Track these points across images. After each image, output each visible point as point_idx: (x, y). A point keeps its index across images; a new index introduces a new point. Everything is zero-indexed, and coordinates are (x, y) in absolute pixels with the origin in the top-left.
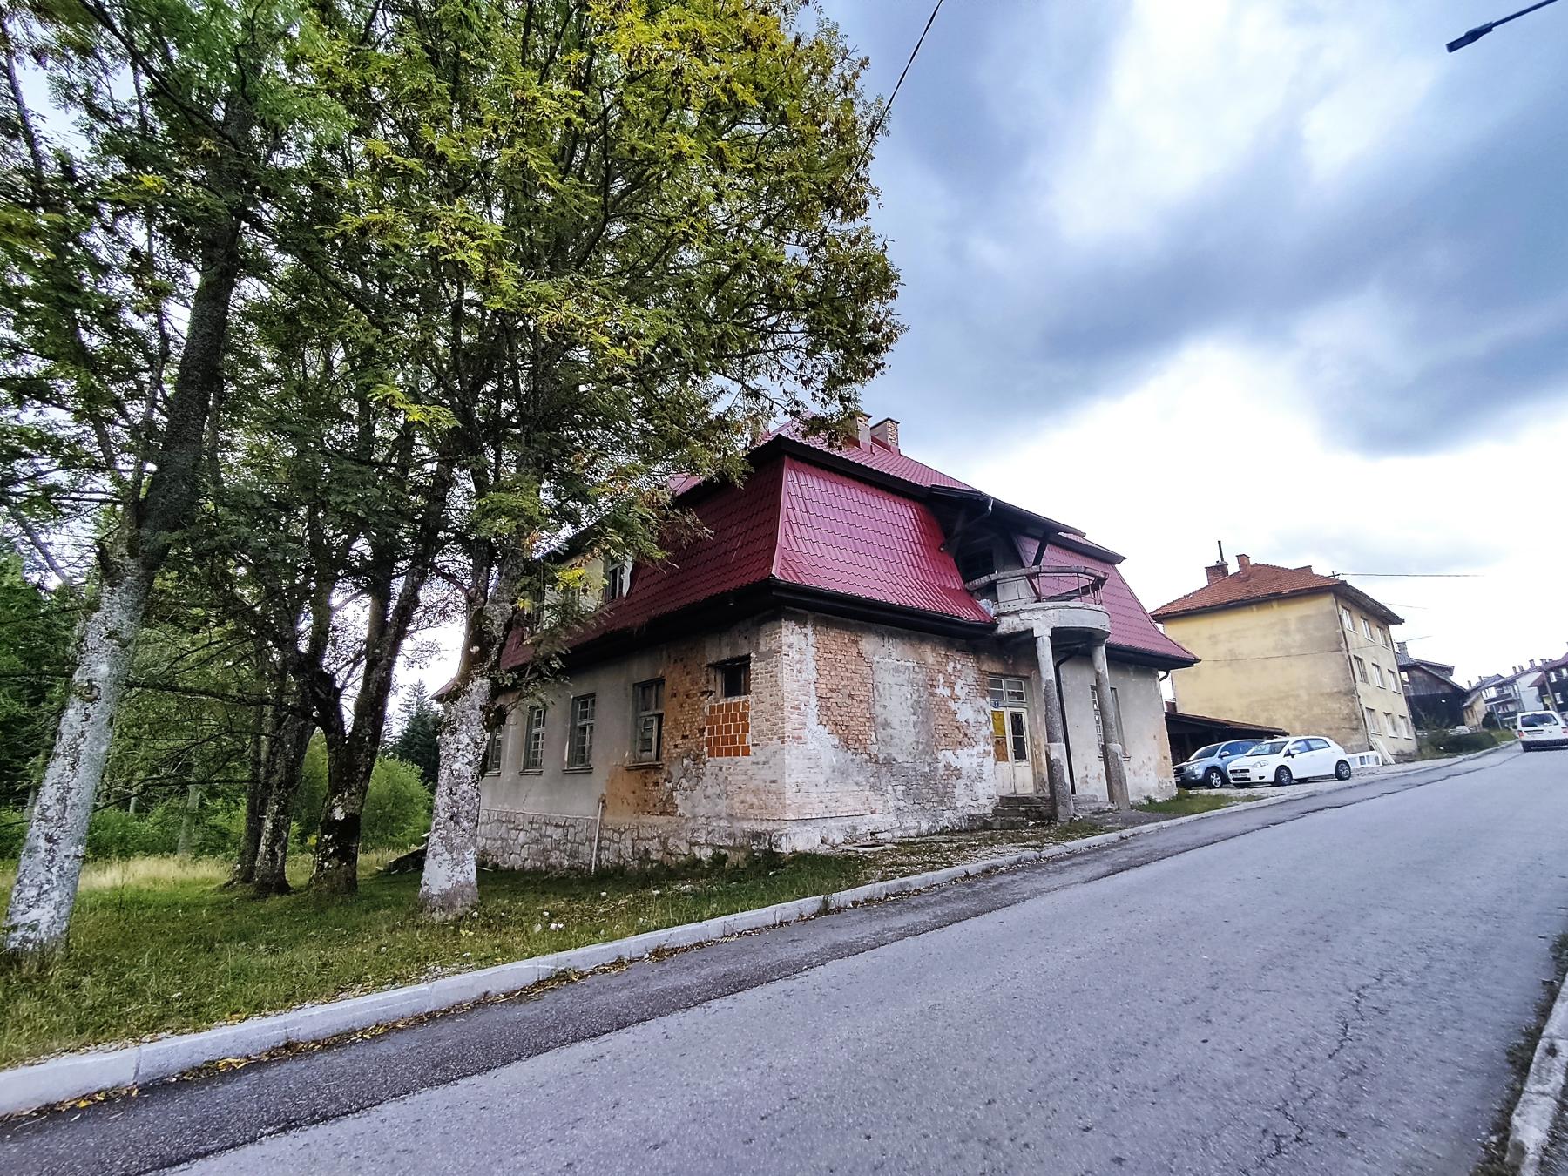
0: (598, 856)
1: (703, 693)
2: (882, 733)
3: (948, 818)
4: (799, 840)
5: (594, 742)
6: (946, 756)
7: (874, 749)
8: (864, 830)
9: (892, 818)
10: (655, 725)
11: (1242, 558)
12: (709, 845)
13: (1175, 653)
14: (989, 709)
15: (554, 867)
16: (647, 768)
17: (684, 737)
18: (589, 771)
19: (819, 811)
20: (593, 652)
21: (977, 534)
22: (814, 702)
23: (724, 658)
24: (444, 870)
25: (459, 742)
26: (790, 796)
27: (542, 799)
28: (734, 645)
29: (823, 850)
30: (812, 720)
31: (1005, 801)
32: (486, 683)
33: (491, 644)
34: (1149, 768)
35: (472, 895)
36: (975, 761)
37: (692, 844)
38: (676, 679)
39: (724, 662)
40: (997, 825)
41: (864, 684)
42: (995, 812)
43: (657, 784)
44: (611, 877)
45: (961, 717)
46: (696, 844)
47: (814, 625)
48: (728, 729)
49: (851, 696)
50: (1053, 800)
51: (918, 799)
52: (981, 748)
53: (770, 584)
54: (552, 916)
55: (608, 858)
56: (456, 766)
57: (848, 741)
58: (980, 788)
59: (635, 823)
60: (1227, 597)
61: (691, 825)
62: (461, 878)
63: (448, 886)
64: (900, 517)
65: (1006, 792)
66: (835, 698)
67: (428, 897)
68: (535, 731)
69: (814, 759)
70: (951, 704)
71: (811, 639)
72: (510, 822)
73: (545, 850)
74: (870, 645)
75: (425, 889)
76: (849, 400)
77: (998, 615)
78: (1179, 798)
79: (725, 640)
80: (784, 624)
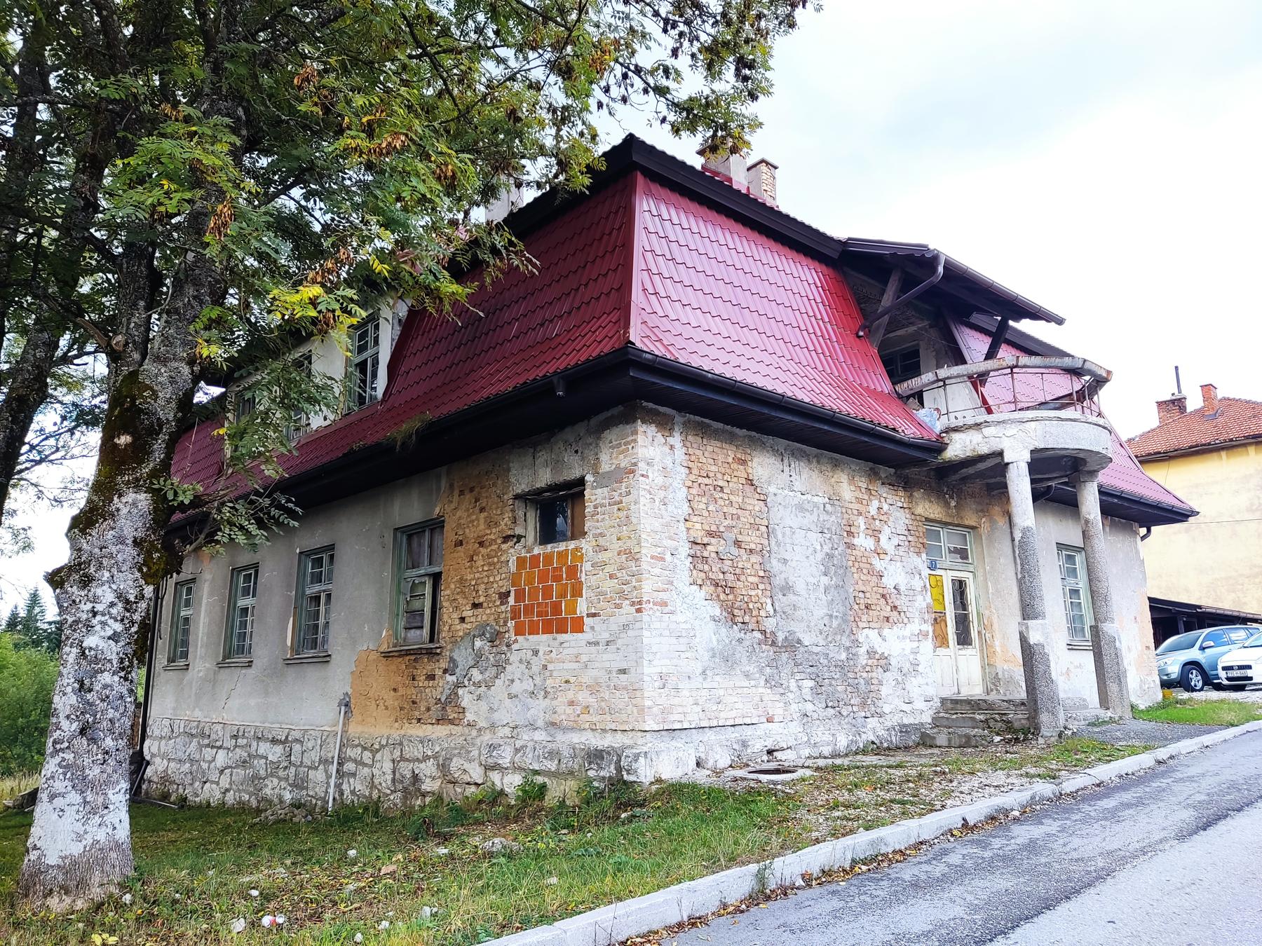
0: (338, 786)
1: (506, 539)
2: (782, 601)
3: (874, 730)
4: (661, 764)
5: (333, 615)
6: (869, 637)
7: (770, 624)
9: (795, 727)
10: (428, 590)
11: (1207, 389)
12: (517, 769)
13: (1167, 500)
14: (926, 572)
15: (270, 802)
16: (418, 651)
17: (476, 606)
18: (326, 659)
19: (694, 718)
20: (332, 482)
21: (916, 306)
22: (685, 549)
23: (541, 484)
24: (70, 822)
25: (96, 600)
26: (651, 695)
27: (252, 702)
28: (557, 464)
29: (702, 777)
31: (952, 705)
32: (143, 500)
33: (154, 432)
34: (1143, 663)
35: (120, 865)
36: (909, 646)
37: (488, 768)
38: (460, 517)
39: (540, 491)
40: (942, 740)
41: (755, 526)
42: (936, 722)
43: (431, 677)
44: (359, 818)
45: (888, 582)
46: (495, 767)
47: (684, 433)
48: (547, 592)
49: (737, 543)
50: (1032, 704)
51: (833, 704)
52: (915, 627)
53: (626, 358)
54: (266, 897)
55: (355, 788)
56: (90, 641)
57: (735, 612)
58: (916, 687)
59: (396, 735)
60: (1186, 441)
61: (487, 738)
62: (101, 836)
63: (76, 849)
64: (801, 281)
65: (948, 692)
66: (715, 545)
67: (39, 870)
68: (242, 603)
70: (876, 561)
71: (680, 452)
72: (203, 735)
73: (256, 777)
75: (33, 855)
76: (751, 66)
77: (949, 430)
78: (1164, 705)
79: (543, 456)
80: (641, 427)
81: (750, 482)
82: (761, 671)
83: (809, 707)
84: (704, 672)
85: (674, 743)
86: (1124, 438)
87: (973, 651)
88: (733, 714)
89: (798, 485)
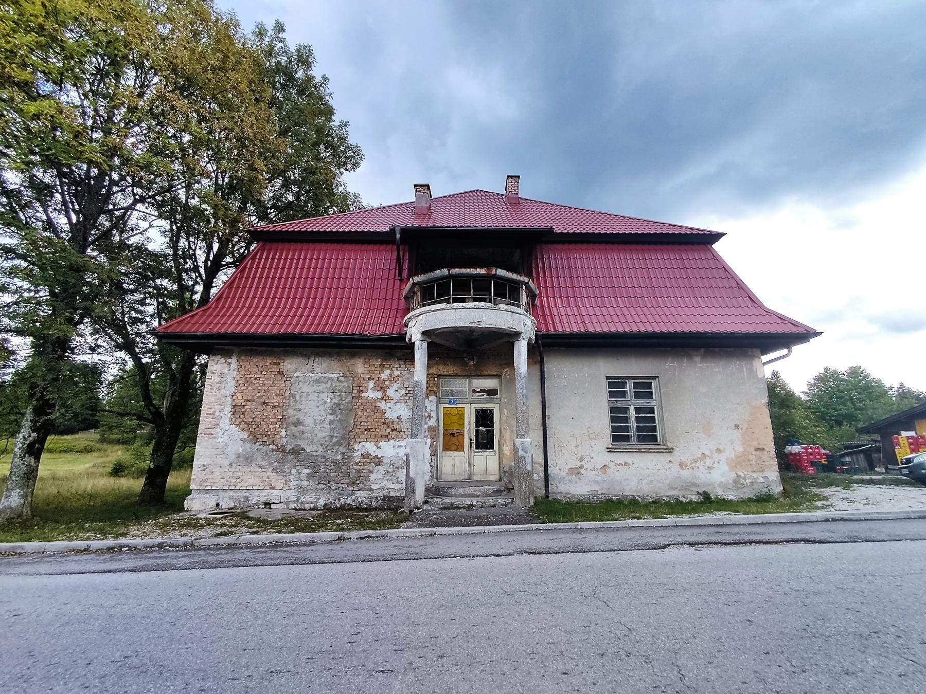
8: (254, 501)
13: (788, 329)
19: (219, 484)
22: (228, 409)
30: (225, 423)
57: (257, 434)
69: (222, 450)
74: (290, 365)
82: (270, 464)
83: (305, 483)
84: (231, 464)
86: (770, 477)
87: (492, 454)
89: (318, 370)
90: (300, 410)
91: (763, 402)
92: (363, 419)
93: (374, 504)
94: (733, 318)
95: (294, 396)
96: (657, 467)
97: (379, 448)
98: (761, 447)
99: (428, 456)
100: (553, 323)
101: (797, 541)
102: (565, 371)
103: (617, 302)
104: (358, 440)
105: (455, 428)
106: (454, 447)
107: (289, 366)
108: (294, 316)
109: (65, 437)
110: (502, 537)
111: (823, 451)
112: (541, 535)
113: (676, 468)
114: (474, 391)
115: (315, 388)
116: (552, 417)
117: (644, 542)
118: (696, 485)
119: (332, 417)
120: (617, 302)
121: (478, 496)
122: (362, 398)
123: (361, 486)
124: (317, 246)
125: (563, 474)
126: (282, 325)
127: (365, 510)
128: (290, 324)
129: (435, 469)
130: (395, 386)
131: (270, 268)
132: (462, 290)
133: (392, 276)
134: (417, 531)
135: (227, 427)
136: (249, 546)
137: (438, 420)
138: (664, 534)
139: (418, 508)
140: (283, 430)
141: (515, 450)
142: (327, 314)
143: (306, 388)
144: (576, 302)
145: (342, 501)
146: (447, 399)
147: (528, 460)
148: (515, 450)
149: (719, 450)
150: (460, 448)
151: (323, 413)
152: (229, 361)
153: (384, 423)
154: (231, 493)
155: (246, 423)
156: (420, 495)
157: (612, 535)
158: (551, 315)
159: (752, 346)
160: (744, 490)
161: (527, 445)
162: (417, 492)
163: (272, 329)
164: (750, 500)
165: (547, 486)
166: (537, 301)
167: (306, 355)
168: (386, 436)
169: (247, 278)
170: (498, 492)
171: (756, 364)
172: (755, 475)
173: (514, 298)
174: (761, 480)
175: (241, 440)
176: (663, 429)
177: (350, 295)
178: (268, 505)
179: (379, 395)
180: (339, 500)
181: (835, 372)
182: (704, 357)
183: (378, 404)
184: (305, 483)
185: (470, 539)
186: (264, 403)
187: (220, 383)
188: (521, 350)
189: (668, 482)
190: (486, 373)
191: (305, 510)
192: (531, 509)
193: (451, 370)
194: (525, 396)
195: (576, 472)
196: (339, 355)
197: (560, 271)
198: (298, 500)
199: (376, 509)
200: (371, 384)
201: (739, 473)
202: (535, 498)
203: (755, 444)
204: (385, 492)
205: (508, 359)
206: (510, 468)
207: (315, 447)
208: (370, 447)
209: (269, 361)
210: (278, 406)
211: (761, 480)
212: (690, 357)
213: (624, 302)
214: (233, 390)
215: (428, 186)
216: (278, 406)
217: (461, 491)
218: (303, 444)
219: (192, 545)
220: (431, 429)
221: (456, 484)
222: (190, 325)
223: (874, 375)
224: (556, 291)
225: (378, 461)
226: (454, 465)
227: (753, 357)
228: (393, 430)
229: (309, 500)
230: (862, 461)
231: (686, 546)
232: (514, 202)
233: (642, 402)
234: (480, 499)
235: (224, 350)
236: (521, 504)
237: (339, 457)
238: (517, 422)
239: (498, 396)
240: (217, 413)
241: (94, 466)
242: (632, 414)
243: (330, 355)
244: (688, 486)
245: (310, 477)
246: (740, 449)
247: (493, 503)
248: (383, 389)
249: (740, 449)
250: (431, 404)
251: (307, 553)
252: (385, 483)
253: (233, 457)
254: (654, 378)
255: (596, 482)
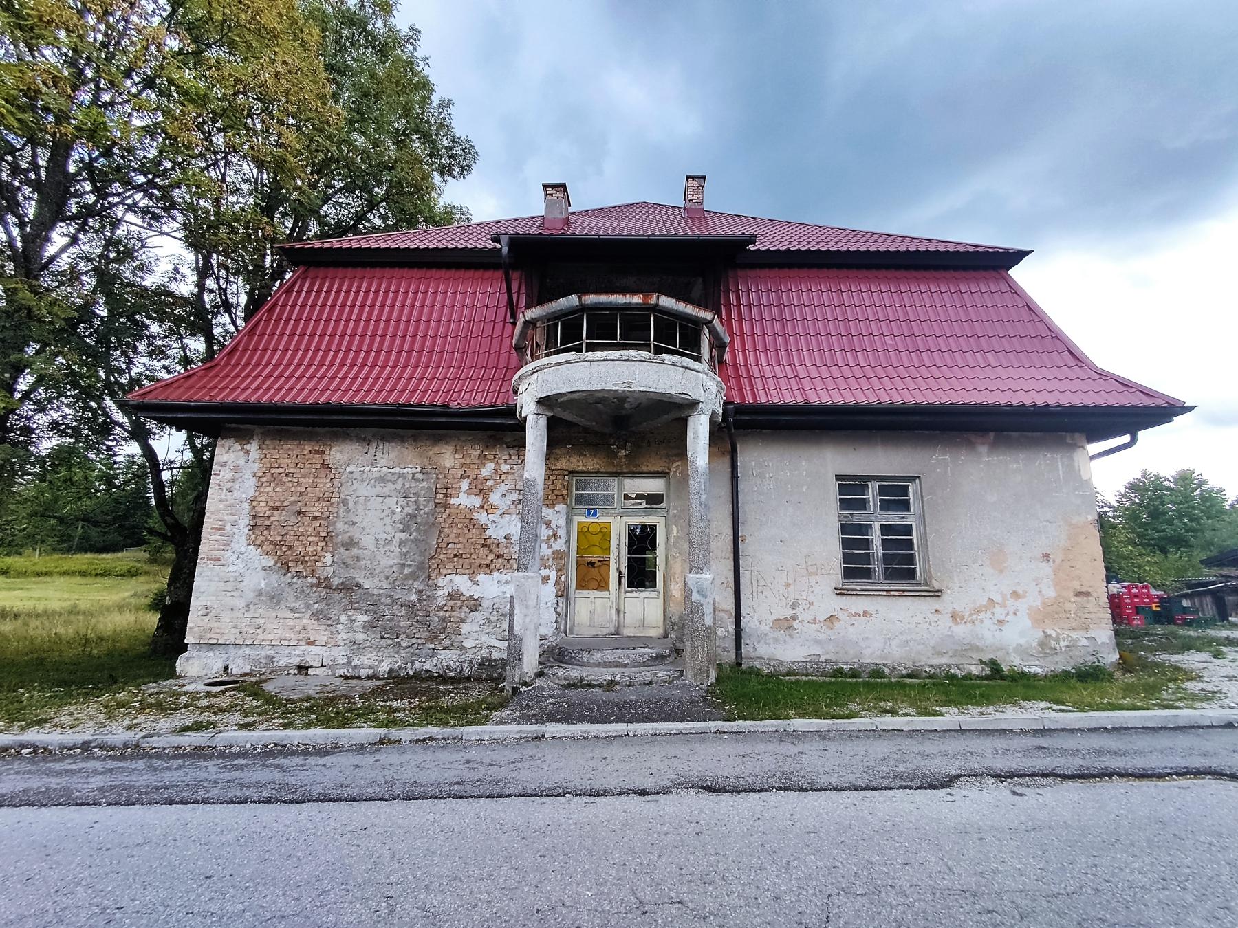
8: (282, 663)
13: (1137, 400)
19: (230, 636)
22: (245, 521)
30: (240, 541)
57: (287, 559)
69: (235, 584)
74: (342, 454)
81: (325, 466)
82: (308, 607)
83: (361, 637)
84: (247, 606)
85: (211, 654)
86: (1098, 639)
87: (654, 595)
88: (271, 637)
89: (382, 462)
90: (354, 524)
91: (1090, 518)
92: (452, 538)
93: (467, 671)
94: (1044, 384)
95: (345, 502)
96: (916, 619)
97: (476, 583)
98: (1084, 590)
99: (553, 597)
100: (752, 389)
101: (1198, 773)
102: (772, 468)
103: (856, 358)
104: (445, 571)
105: (595, 555)
106: (594, 584)
107: (338, 456)
108: (345, 378)
109: (104, 556)
110: (657, 748)
111: (1153, 592)
112: (723, 748)
113: (945, 621)
114: (627, 497)
115: (378, 490)
116: (748, 539)
117: (911, 767)
118: (978, 649)
119: (403, 536)
120: (856, 358)
121: (625, 666)
122: (449, 506)
123: (447, 642)
124: (388, 272)
125: (765, 628)
126: (324, 391)
127: (453, 680)
128: (336, 390)
129: (564, 619)
130: (502, 488)
131: (314, 306)
132: (605, 331)
133: (500, 318)
134: (513, 729)
135: (243, 549)
136: (227, 755)
137: (568, 542)
138: (943, 748)
139: (526, 684)
140: (329, 555)
141: (687, 592)
142: (395, 375)
143: (363, 490)
144: (789, 357)
145: (417, 665)
146: (583, 508)
147: (708, 610)
148: (687, 592)
149: (1015, 595)
150: (603, 585)
151: (389, 528)
152: (248, 447)
153: (484, 546)
154: (248, 651)
155: (271, 543)
156: (530, 664)
157: (849, 748)
158: (749, 377)
159: (1073, 429)
160: (1057, 658)
161: (706, 584)
162: (525, 659)
163: (307, 397)
164: (1067, 674)
165: (738, 646)
166: (727, 356)
167: (364, 439)
168: (487, 566)
169: (278, 320)
170: (659, 659)
171: (1079, 457)
172: (1074, 635)
173: (690, 346)
174: (1084, 642)
175: (264, 569)
176: (926, 560)
177: (423, 342)
178: (303, 669)
179: (477, 501)
180: (413, 663)
181: (1158, 477)
182: (994, 445)
183: (476, 516)
184: (361, 637)
185: (601, 750)
186: (299, 513)
187: (233, 481)
188: (699, 430)
189: (932, 643)
190: (645, 469)
191: (359, 678)
192: (711, 690)
193: (588, 463)
194: (705, 506)
195: (786, 625)
196: (415, 439)
197: (765, 311)
198: (349, 662)
199: (468, 679)
200: (465, 485)
201: (1049, 631)
202: (719, 666)
203: (1076, 585)
204: (484, 653)
205: (677, 445)
206: (681, 618)
207: (376, 580)
208: (462, 583)
209: (308, 448)
210: (321, 518)
211: (1084, 642)
212: (971, 445)
213: (866, 359)
214: (252, 492)
215: (564, 186)
216: (321, 518)
217: (598, 656)
218: (358, 577)
219: (137, 746)
220: (557, 555)
221: (590, 646)
222: (182, 389)
223: (1214, 482)
224: (759, 340)
225: (474, 604)
226: (593, 612)
227: (1074, 446)
228: (498, 557)
229: (367, 662)
230: (1209, 608)
231: (990, 781)
232: (697, 214)
233: (893, 517)
234: (627, 671)
235: (239, 430)
236: (697, 676)
237: (414, 597)
238: (691, 547)
239: (663, 505)
240: (228, 528)
241: (135, 595)
242: (876, 535)
243: (402, 439)
244: (966, 650)
245: (368, 627)
246: (1051, 593)
247: (648, 679)
248: (483, 492)
249: (1051, 593)
250: (557, 515)
251: (316, 774)
252: (484, 638)
253: (251, 595)
254: (912, 479)
255: (817, 642)
